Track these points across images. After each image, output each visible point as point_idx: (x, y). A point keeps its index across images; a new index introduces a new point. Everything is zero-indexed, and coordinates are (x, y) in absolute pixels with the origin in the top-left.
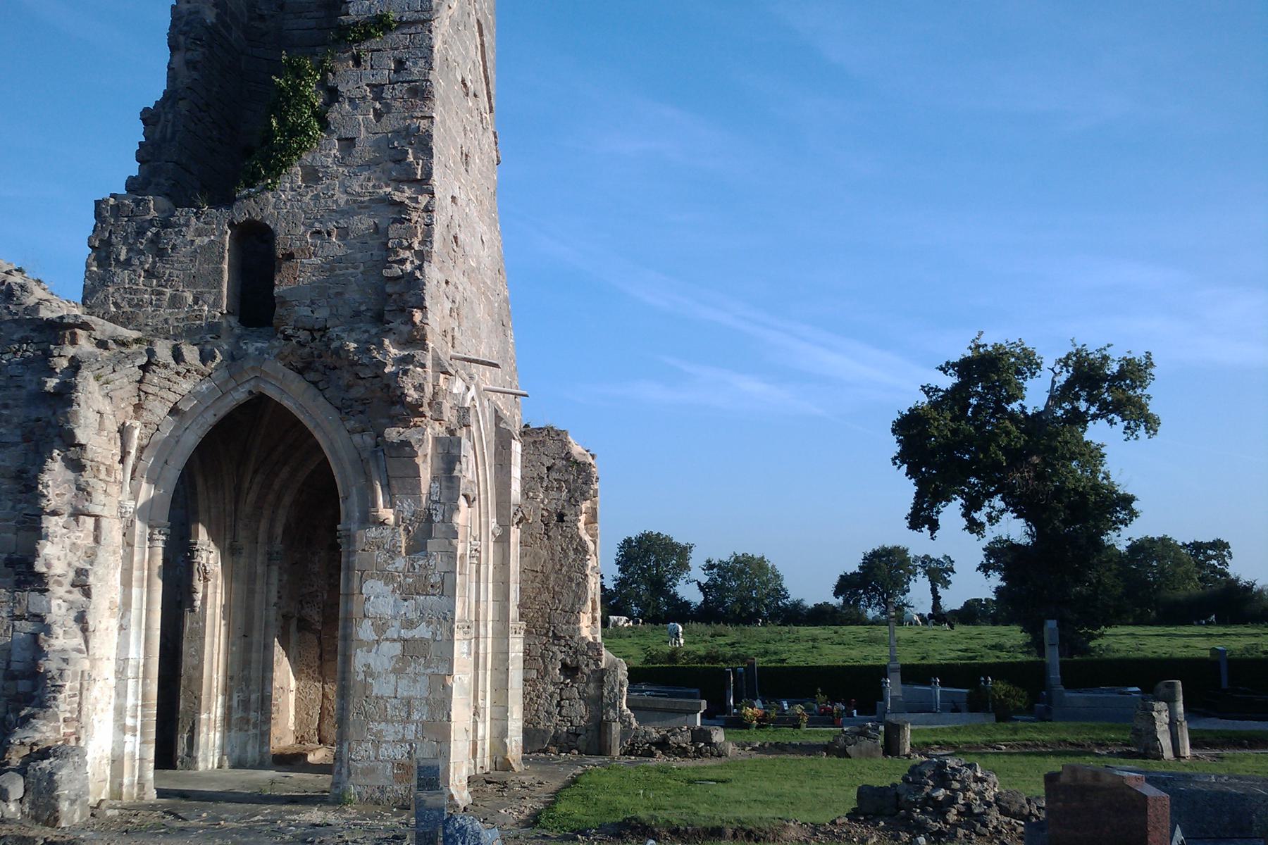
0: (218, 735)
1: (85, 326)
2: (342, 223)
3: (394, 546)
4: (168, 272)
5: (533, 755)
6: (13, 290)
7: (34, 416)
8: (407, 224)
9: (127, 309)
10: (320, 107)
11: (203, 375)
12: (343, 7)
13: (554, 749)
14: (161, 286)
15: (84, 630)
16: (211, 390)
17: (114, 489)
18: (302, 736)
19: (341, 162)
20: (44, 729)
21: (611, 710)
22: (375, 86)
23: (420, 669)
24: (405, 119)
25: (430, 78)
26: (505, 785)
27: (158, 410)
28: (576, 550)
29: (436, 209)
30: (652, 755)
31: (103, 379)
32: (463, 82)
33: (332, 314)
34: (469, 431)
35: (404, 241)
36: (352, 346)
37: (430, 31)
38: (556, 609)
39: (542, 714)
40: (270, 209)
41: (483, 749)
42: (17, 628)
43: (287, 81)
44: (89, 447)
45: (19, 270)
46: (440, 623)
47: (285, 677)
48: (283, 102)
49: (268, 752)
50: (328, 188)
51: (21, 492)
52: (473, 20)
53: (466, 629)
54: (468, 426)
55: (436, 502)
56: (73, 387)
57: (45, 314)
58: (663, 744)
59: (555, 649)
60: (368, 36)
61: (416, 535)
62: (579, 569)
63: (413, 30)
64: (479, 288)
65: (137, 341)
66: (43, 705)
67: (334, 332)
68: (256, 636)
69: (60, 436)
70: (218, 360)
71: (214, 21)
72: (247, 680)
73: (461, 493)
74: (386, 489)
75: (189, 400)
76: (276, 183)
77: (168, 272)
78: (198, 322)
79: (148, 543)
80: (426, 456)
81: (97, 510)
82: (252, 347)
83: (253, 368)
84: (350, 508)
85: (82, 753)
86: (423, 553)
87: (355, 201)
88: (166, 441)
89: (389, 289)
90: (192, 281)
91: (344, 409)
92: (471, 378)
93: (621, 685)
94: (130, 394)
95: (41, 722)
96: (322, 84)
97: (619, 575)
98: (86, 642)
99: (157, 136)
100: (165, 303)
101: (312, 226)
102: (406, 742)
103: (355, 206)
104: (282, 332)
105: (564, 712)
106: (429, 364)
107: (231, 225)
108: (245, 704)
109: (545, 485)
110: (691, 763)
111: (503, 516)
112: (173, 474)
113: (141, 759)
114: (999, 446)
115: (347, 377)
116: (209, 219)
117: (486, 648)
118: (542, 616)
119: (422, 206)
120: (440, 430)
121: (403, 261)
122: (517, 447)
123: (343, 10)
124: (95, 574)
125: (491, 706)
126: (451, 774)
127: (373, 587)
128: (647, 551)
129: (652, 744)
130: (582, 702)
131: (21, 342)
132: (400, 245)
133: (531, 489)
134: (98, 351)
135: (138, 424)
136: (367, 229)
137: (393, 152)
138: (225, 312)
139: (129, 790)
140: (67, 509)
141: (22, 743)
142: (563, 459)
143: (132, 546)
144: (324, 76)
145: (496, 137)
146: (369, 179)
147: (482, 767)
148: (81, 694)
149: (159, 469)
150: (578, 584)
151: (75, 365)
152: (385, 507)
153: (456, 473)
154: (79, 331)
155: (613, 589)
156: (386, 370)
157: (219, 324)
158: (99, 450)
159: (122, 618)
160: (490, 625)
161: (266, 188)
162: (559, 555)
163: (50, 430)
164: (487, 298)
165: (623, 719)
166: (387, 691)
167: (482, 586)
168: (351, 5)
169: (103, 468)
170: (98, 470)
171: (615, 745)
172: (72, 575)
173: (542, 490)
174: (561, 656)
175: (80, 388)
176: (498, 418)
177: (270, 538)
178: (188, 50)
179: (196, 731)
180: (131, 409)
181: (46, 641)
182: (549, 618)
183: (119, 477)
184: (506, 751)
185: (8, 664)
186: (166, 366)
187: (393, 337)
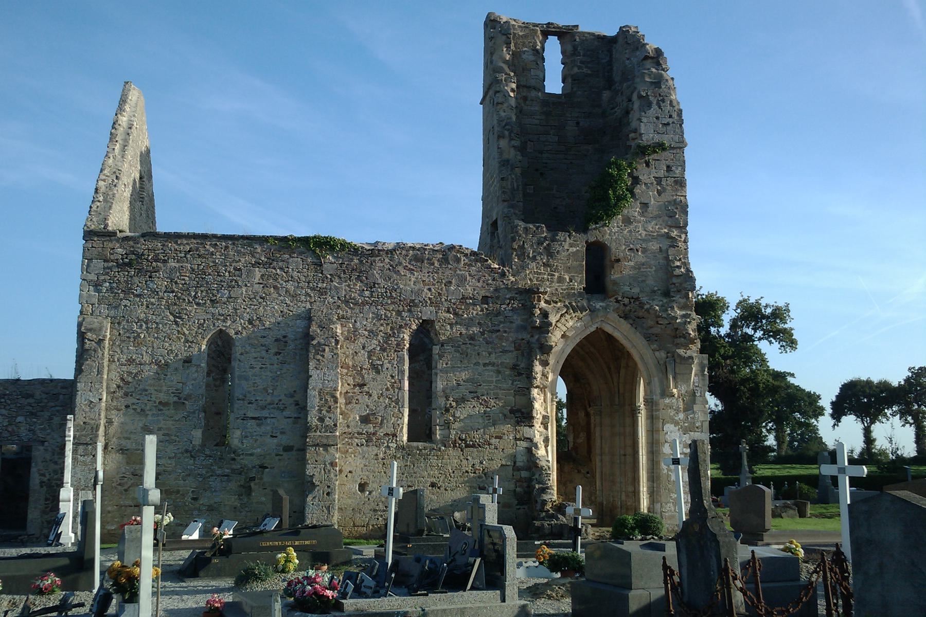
2: (644, 246)
7: (520, 337)
14: (552, 271)
22: (657, 178)
24: (673, 196)
40: (607, 236)
50: (636, 227)
55: (696, 386)
63: (675, 152)
75: (571, 331)
87: (650, 235)
91: (649, 338)
100: (555, 280)
114: (720, 354)
119: (683, 239)
127: (669, 427)
137: (668, 212)
144: (632, 171)
146: (656, 225)
161: (605, 225)
185: (515, 463)
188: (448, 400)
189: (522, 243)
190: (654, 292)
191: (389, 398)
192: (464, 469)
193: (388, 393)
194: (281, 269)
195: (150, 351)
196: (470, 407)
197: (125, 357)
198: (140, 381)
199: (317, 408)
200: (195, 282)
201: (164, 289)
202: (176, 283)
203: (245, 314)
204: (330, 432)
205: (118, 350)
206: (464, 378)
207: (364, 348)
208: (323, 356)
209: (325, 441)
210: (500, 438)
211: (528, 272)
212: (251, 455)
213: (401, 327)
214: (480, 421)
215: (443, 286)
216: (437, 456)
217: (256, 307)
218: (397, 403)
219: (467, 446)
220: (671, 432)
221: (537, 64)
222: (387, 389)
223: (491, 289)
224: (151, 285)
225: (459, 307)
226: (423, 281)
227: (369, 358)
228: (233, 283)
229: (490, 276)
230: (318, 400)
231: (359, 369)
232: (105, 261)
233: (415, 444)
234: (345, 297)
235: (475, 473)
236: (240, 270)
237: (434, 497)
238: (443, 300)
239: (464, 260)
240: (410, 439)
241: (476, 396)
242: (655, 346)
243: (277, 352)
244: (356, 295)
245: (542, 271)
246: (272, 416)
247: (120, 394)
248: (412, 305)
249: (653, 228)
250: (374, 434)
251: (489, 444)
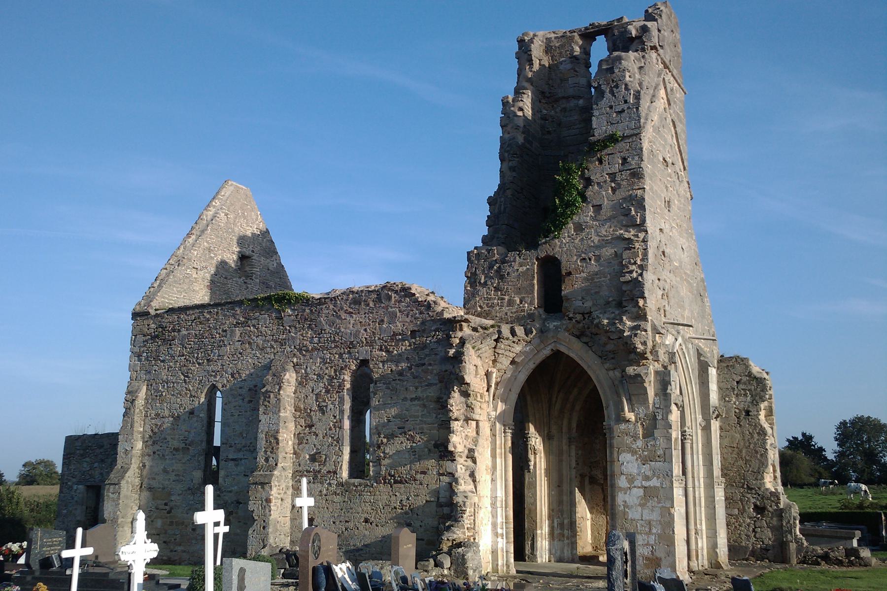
0: (547, 543)
1: (466, 321)
2: (597, 253)
3: (635, 433)
4: (506, 287)
5: (739, 562)
6: (430, 304)
8: (633, 250)
9: (486, 309)
10: (581, 189)
11: (527, 342)
12: (592, 131)
13: (752, 558)
14: (503, 295)
15: (474, 481)
16: (532, 350)
17: (485, 406)
18: (596, 547)
19: (594, 219)
20: (458, 532)
21: (789, 535)
22: (611, 174)
23: (655, 504)
24: (629, 191)
25: (642, 166)
26: (716, 576)
27: (505, 362)
28: (759, 434)
29: (649, 240)
30: (819, 564)
31: (476, 348)
32: (664, 159)
33: (594, 304)
34: (676, 366)
35: (632, 260)
36: (606, 321)
37: (641, 140)
38: (748, 471)
39: (744, 537)
40: (557, 249)
41: (703, 555)
42: (441, 480)
43: (563, 177)
44: (471, 384)
45: (433, 293)
46: (664, 478)
47: (583, 511)
48: (560, 189)
49: (576, 554)
51: (440, 409)
52: (669, 120)
53: (680, 481)
54: (675, 363)
55: (657, 408)
56: (463, 353)
57: (446, 315)
58: (826, 557)
59: (749, 496)
60: (606, 147)
61: (647, 427)
62: (761, 445)
63: (630, 140)
64: (681, 278)
65: (492, 326)
66: (457, 520)
67: (595, 314)
68: (565, 487)
69: (457, 379)
70: (534, 334)
71: (523, 141)
72: (561, 512)
73: (672, 403)
74: (629, 402)
75: (521, 356)
76: (560, 234)
77: (506, 287)
78: (522, 313)
79: (503, 434)
80: (650, 382)
81: (477, 417)
82: (552, 325)
83: (553, 337)
84: (609, 412)
85: (478, 546)
86: (652, 438)
87: (603, 240)
88: (509, 379)
89: (624, 288)
90: (519, 291)
91: (603, 357)
92: (678, 333)
93: (795, 519)
94: (490, 355)
95: (456, 529)
96: (582, 176)
97: (838, 449)
98: (476, 487)
99: (496, 211)
100: (505, 304)
101: (580, 256)
102: (649, 545)
103: (604, 243)
104: (567, 316)
105: (757, 536)
106: (649, 329)
107: (537, 259)
108: (561, 525)
109: (735, 392)
110: (844, 569)
111: (706, 414)
112: (514, 397)
113: (507, 552)
115: (604, 339)
116: (526, 257)
117: (700, 494)
118: (739, 475)
119: (641, 239)
120: (658, 366)
121: (631, 272)
122: (713, 372)
123: (591, 134)
124: (478, 451)
125: (706, 529)
126: (677, 565)
128: (859, 430)
129: (819, 557)
130: (769, 529)
131: (435, 331)
132: (630, 263)
133: (727, 396)
134: (473, 333)
135: (494, 370)
136: (610, 255)
138: (536, 307)
139: (502, 569)
140: (463, 417)
141: (448, 540)
142: (747, 376)
143: (496, 436)
145: (689, 184)
147: (703, 566)
148: (474, 515)
149: (507, 394)
150: (762, 455)
151: (463, 342)
152: (629, 412)
153: (668, 391)
154: (463, 323)
155: (834, 459)
156: (625, 335)
157: (533, 314)
158: (477, 385)
159: (492, 475)
160: (702, 480)
161: (555, 237)
162: (747, 437)
163: (452, 376)
164: (688, 282)
165: (797, 541)
166: (637, 516)
167: (695, 457)
168: (595, 130)
169: (478, 395)
170: (476, 396)
171: (793, 557)
172: (466, 451)
173: (734, 396)
174: (753, 500)
175: (465, 354)
176: (699, 354)
177: (570, 429)
178: (510, 161)
179: (535, 540)
180: (491, 362)
181: (456, 487)
182: (744, 476)
183: (487, 399)
184: (717, 557)
185: (438, 499)
186: (507, 339)
187: (628, 315)
188: (380, 437)
189: (474, 269)
190: (608, 303)
191: (332, 437)
192: (393, 505)
193: (331, 432)
194: (254, 326)
195: (168, 406)
196: (398, 443)
197: (154, 412)
198: (162, 431)
199: (263, 450)
200: (197, 346)
201: (178, 353)
202: (186, 348)
203: (229, 369)
204: (270, 471)
205: (150, 407)
206: (393, 414)
207: (313, 391)
208: (269, 402)
209: (262, 480)
210: (424, 473)
211: (478, 299)
212: (230, 492)
213: (342, 368)
214: (407, 456)
215: (377, 325)
216: (370, 492)
217: (236, 362)
218: (338, 442)
219: (396, 482)
220: (628, 463)
221: (576, 71)
222: (330, 429)
223: (418, 322)
224: (171, 352)
225: (390, 344)
226: (361, 322)
227: (317, 401)
228: (221, 343)
229: (417, 310)
230: (264, 442)
231: (309, 411)
232: (144, 336)
233: (353, 480)
234: (299, 345)
235: (402, 509)
236: (225, 331)
237: (367, 533)
238: (377, 338)
239: (395, 297)
240: (351, 476)
241: (403, 430)
242: (608, 364)
243: (249, 401)
244: (308, 342)
245: (493, 296)
246: (245, 457)
247: (150, 443)
248: (352, 345)
249: (606, 231)
250: (319, 472)
251: (415, 480)
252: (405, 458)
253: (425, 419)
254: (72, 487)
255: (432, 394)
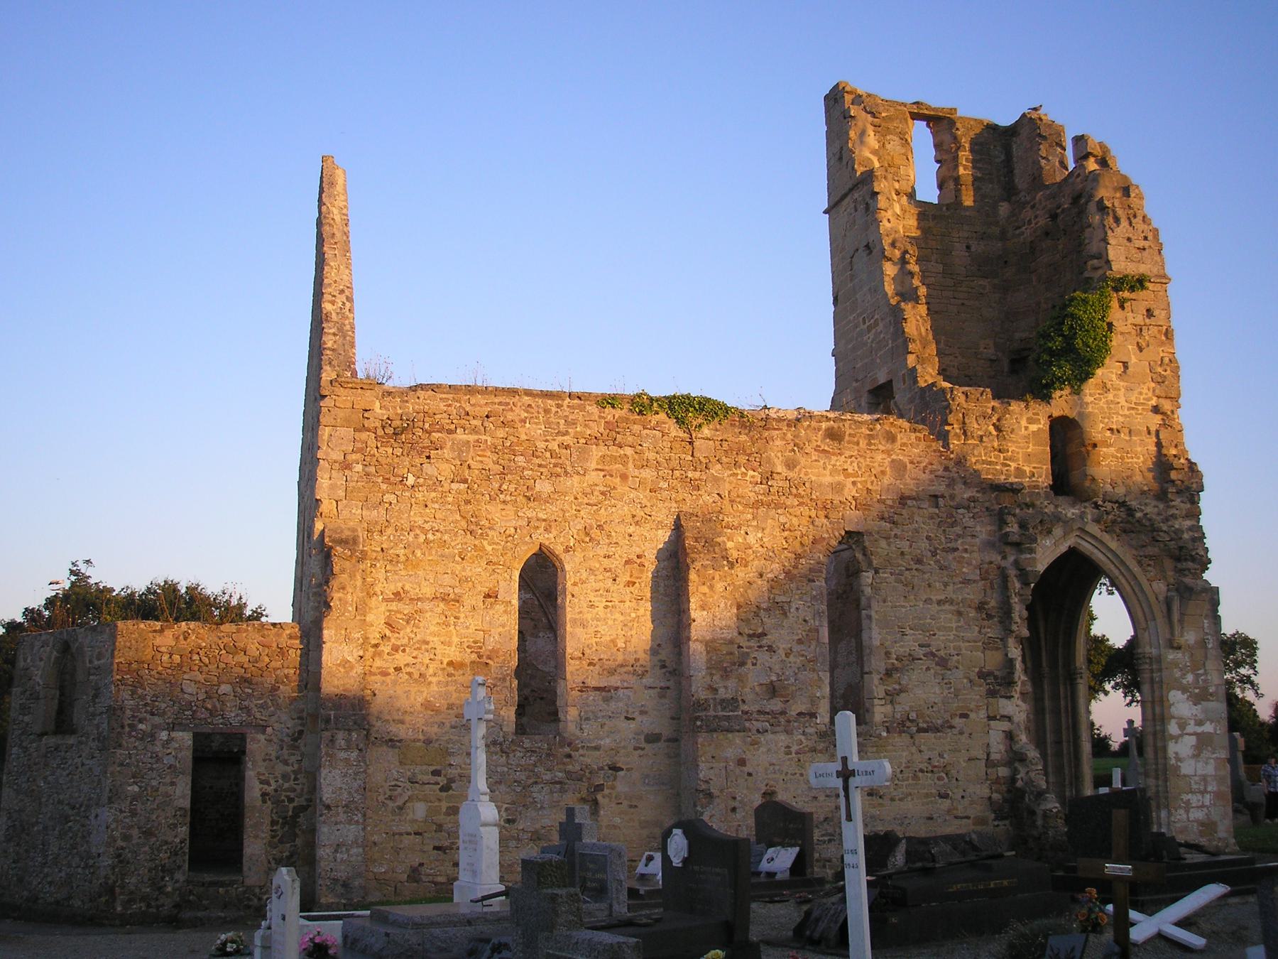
185: (988, 755)
212: (597, 748)
219: (920, 730)
252: (934, 693)
253: (962, 634)
254: (153, 736)
255: (972, 597)
